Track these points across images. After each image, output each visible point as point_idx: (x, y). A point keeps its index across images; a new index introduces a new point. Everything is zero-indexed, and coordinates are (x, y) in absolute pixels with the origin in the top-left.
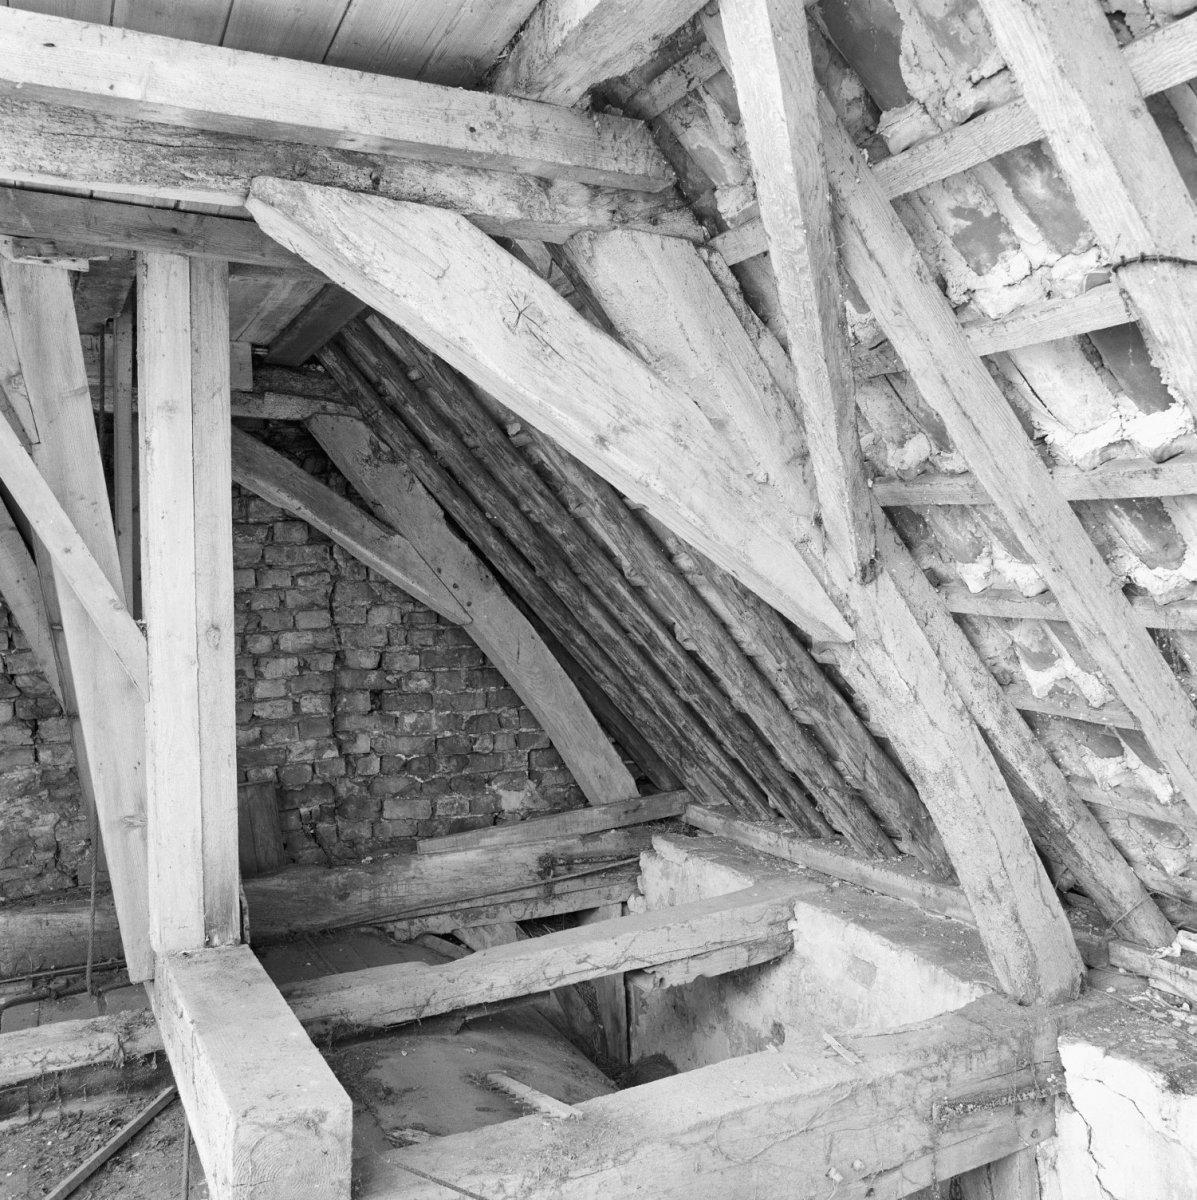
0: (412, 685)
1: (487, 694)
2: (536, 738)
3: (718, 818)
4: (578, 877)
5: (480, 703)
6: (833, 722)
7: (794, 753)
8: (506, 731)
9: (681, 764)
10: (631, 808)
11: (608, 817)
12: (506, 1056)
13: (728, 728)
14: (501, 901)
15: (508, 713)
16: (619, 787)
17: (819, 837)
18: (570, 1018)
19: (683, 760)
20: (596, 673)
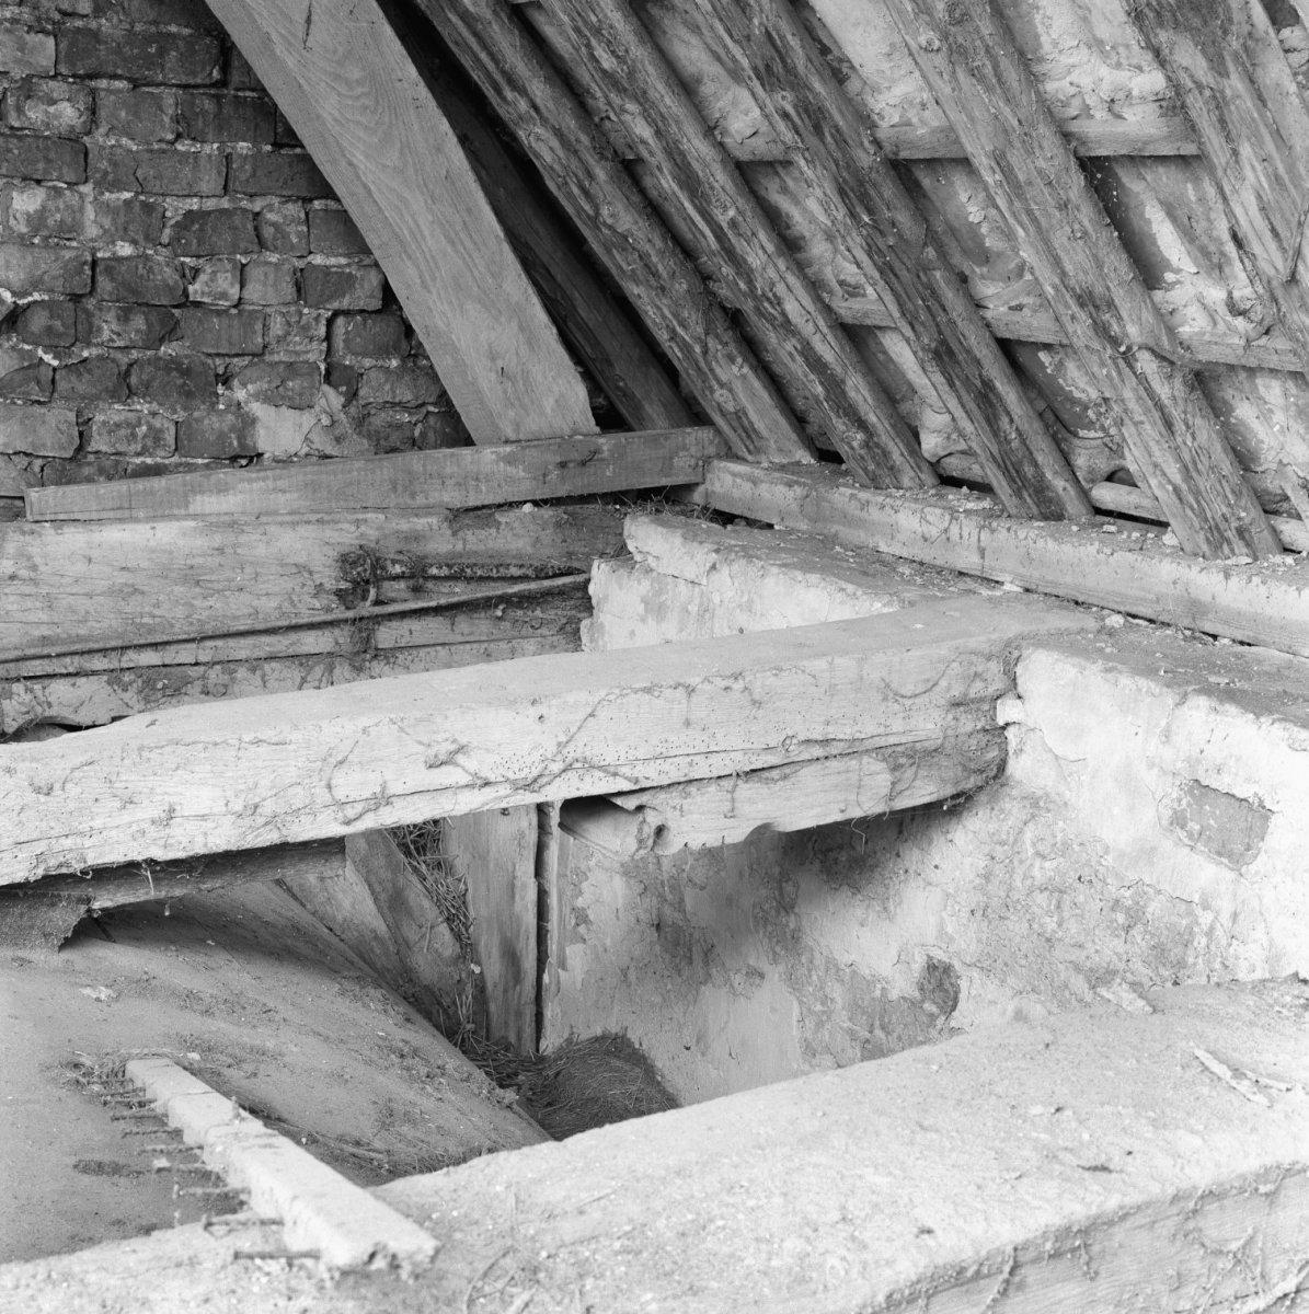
0: (35, 113)
1: (228, 157)
2: (345, 282)
3: (790, 485)
4: (437, 610)
5: (210, 181)
6: (1235, 84)
7: (1060, 239)
8: (274, 258)
9: (705, 352)
10: (576, 456)
11: (519, 472)
12: (207, 1012)
13: (864, 199)
14: (242, 655)
15: (280, 213)
16: (549, 404)
17: (1059, 517)
18: (403, 946)
19: (712, 343)
20: (509, 94)
